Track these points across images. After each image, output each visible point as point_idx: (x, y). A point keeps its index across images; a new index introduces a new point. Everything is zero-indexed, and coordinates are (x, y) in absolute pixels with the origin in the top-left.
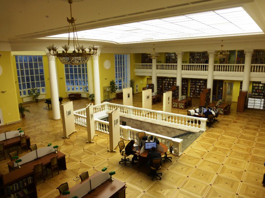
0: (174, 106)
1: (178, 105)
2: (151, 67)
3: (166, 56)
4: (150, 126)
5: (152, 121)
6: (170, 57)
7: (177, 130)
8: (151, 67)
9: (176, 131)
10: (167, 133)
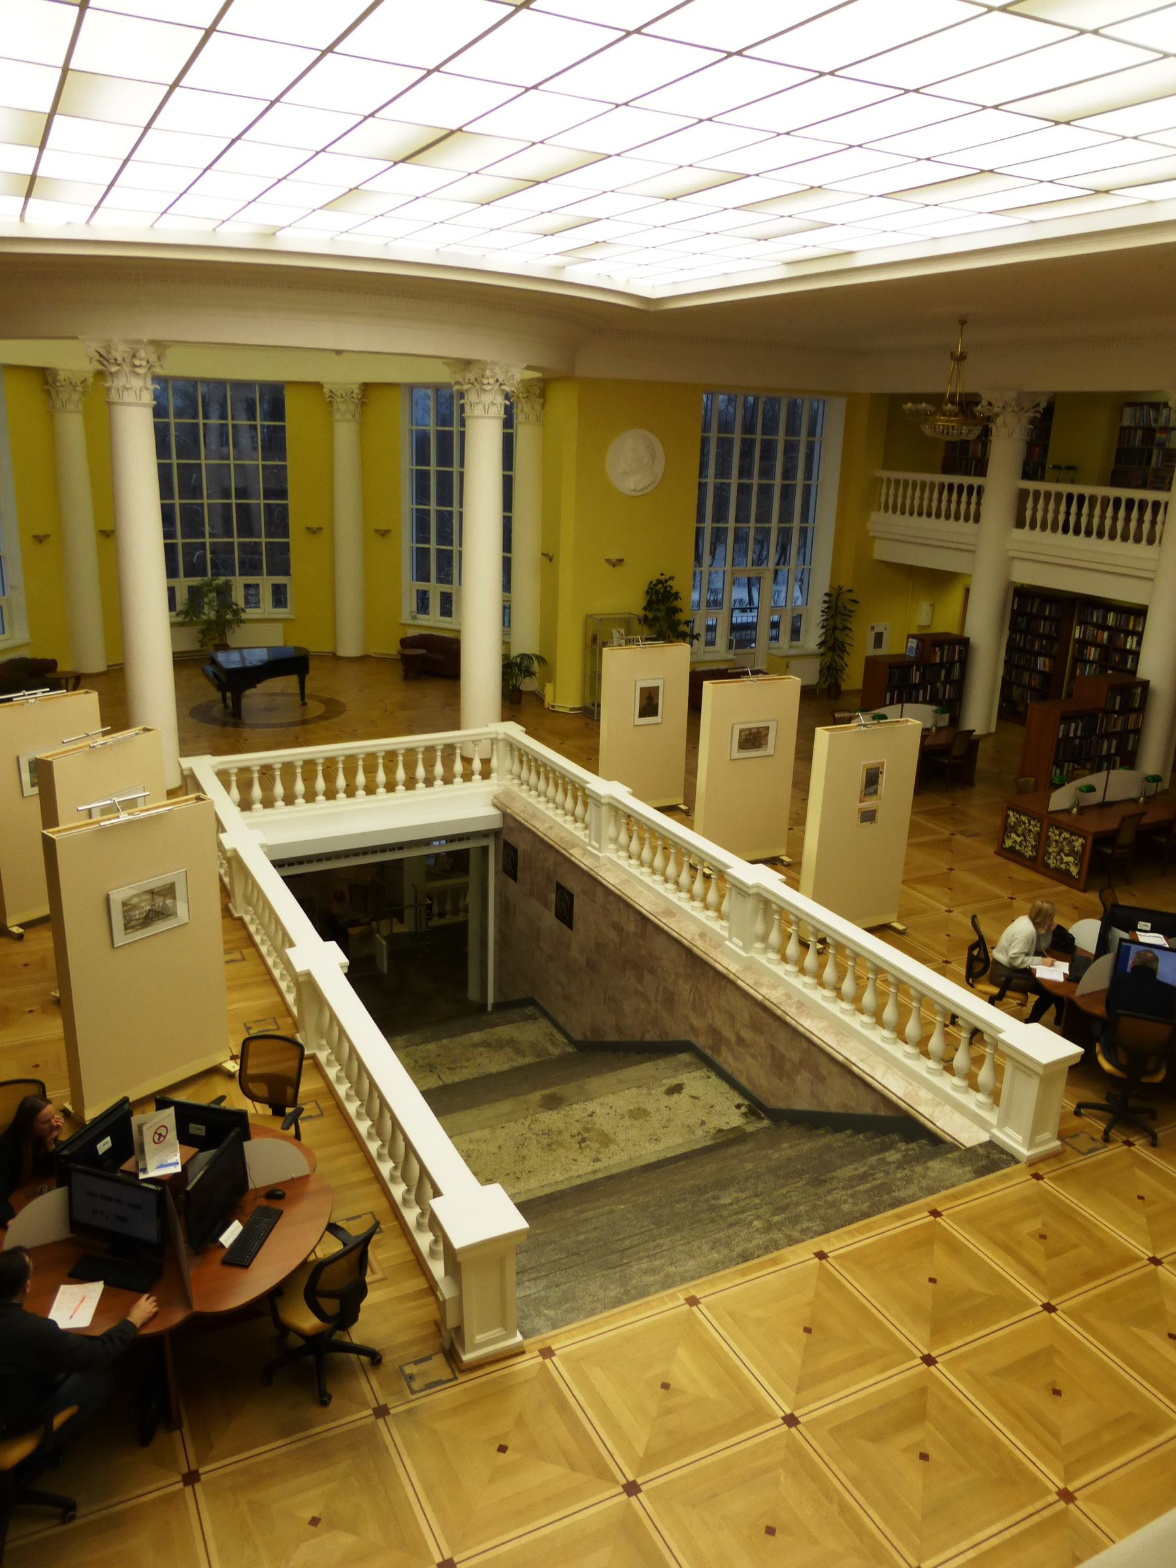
0: (1008, 843)
1: (1042, 841)
2: (1153, 522)
3: (1123, 429)
4: (681, 970)
5: (702, 935)
6: (1149, 433)
7: (835, 1070)
8: (1153, 522)
9: (825, 1073)
10: (769, 1061)
